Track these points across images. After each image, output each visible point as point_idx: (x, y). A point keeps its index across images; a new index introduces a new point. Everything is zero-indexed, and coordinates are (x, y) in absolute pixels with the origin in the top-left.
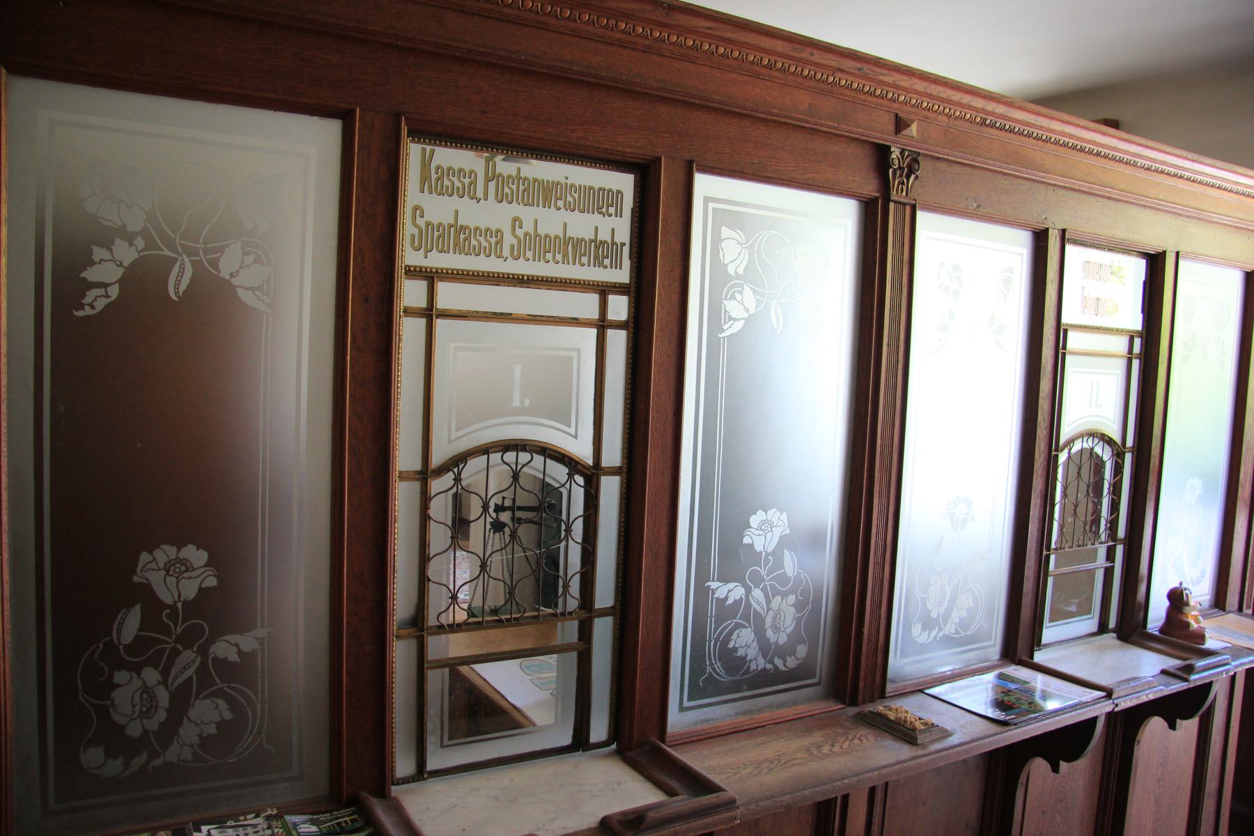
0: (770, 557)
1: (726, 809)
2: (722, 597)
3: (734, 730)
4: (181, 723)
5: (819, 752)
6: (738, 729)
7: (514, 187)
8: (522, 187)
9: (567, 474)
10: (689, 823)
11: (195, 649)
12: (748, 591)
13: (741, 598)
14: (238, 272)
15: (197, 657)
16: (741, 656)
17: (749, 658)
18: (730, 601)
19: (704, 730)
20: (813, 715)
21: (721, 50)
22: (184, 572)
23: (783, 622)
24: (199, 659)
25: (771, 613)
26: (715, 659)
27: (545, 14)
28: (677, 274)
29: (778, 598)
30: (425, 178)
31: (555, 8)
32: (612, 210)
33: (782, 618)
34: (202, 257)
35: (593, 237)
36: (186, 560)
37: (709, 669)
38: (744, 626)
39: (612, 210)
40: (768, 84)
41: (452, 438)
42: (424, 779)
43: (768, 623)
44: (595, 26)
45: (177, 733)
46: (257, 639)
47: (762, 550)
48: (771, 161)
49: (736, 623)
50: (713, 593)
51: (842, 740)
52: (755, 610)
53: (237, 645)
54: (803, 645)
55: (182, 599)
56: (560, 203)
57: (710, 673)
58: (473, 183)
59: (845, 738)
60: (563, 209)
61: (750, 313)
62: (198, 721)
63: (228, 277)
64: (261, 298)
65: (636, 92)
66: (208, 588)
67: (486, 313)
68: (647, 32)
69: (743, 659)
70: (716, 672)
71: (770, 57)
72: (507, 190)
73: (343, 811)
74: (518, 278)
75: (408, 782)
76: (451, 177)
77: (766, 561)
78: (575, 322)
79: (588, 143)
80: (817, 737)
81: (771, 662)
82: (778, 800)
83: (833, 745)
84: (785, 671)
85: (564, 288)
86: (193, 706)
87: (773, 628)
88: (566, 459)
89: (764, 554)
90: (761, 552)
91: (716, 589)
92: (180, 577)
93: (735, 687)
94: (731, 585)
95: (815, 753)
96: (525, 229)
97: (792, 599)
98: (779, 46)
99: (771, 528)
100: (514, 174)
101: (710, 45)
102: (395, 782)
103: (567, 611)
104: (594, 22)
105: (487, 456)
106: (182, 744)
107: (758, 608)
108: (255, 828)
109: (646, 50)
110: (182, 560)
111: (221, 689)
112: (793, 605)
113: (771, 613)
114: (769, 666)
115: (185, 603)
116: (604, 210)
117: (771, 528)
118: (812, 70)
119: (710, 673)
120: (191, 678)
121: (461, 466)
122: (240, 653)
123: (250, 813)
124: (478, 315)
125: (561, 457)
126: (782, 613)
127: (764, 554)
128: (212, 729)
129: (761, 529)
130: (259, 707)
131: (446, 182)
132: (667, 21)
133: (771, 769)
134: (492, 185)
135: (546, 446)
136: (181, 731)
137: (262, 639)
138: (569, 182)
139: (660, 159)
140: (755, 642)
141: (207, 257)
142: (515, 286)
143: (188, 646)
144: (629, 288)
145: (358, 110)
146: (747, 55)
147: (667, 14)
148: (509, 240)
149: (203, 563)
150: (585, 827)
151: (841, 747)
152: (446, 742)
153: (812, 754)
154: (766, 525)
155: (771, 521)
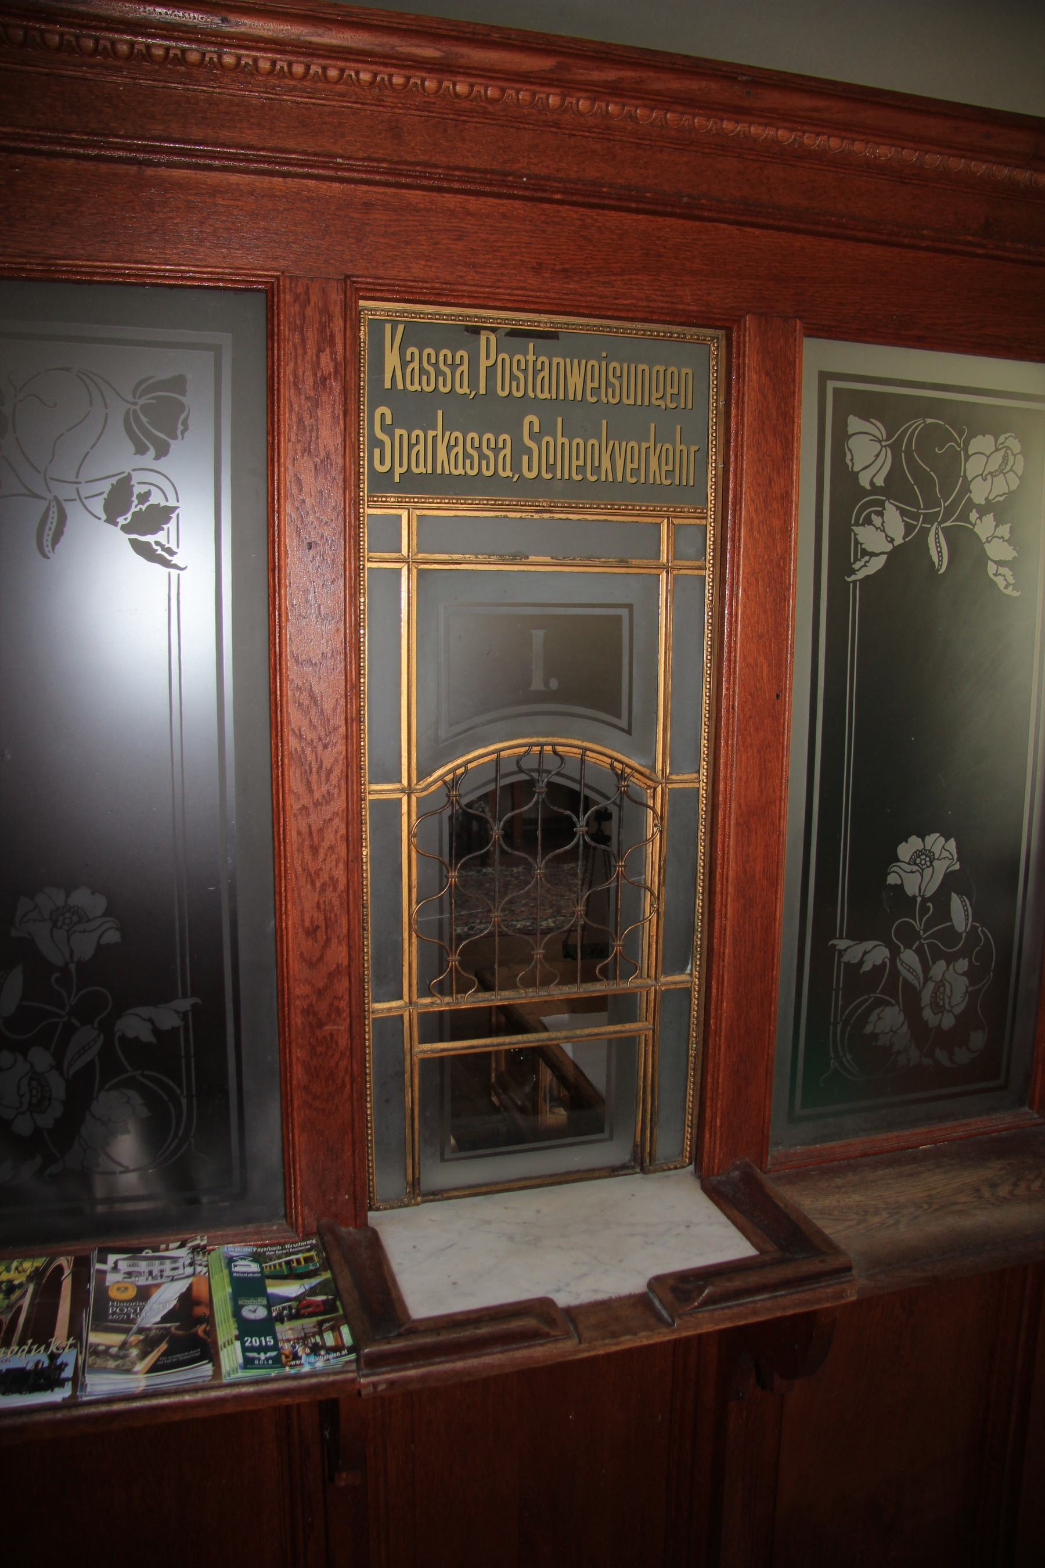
0: (930, 904)
2: (855, 961)
11: (96, 1025)
12: (895, 952)
13: (884, 964)
18: (867, 967)
22: (76, 924)
23: (950, 998)
24: (102, 1036)
25: (931, 986)
29: (942, 964)
38: (889, 1004)
43: (926, 996)
46: (177, 1012)
47: (917, 894)
52: (905, 980)
53: (150, 1020)
55: (75, 960)
61: (896, 543)
77: (924, 910)
83: (1015, 1185)
89: (919, 899)
90: (915, 897)
91: (846, 950)
94: (869, 945)
97: (963, 965)
99: (931, 862)
107: (910, 978)
108: (175, 1262)
112: (964, 974)
113: (931, 986)
122: (156, 1031)
126: (948, 986)
127: (919, 899)
129: (915, 864)
130: (184, 1101)
137: (185, 1014)
149: (100, 911)
154: (923, 857)
155: (930, 851)
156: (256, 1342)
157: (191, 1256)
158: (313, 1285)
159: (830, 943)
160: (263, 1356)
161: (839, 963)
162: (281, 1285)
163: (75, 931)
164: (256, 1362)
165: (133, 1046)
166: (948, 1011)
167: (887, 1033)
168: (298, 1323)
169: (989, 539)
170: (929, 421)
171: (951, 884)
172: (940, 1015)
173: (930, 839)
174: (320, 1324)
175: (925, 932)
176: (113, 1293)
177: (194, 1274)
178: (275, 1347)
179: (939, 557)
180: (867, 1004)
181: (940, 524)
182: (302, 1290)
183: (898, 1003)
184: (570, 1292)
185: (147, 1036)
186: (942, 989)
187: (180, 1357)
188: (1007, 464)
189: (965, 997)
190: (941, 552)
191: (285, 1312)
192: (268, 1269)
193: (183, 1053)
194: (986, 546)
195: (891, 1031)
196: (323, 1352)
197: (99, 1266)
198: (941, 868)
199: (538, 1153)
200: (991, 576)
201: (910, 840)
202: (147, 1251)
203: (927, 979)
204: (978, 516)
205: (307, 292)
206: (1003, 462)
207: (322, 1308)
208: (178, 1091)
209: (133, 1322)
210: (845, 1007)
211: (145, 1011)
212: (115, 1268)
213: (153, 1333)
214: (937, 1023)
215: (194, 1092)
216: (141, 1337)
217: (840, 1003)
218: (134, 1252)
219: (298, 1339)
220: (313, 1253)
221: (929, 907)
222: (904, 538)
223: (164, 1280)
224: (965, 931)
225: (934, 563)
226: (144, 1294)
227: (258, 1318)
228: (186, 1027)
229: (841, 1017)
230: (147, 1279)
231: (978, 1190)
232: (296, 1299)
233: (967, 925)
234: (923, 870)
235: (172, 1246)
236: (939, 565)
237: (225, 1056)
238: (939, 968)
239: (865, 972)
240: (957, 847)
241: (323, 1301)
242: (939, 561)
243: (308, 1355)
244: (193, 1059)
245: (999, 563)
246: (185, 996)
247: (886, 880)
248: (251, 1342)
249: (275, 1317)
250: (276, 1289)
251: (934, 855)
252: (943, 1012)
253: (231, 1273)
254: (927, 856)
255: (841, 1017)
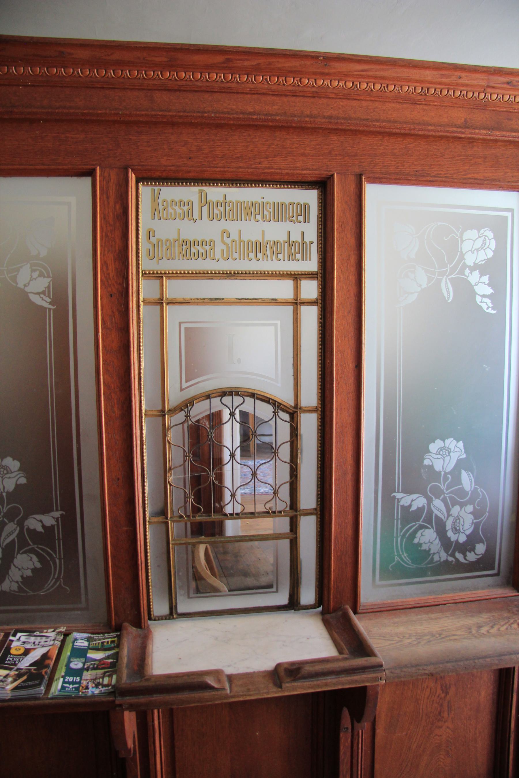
0: (449, 476)
1: (373, 671)
2: (407, 504)
3: (418, 605)
4: (9, 568)
5: (477, 632)
6: (421, 605)
7: (222, 209)
8: (227, 208)
9: (229, 414)
10: (339, 677)
11: (15, 522)
12: (430, 501)
13: (424, 506)
14: (29, 283)
15: (17, 527)
16: (425, 550)
17: (432, 552)
18: (414, 508)
19: (393, 603)
20: (490, 599)
21: (378, 86)
22: (6, 474)
23: (463, 525)
24: (18, 528)
25: (451, 519)
26: (402, 551)
27: (228, 82)
28: (353, 261)
29: (457, 508)
30: (155, 210)
31: (234, 76)
32: (301, 218)
33: (462, 523)
34: (6, 275)
35: (176, 237)
36: (7, 466)
37: (397, 558)
38: (427, 528)
39: (301, 218)
40: (425, 107)
41: (183, 387)
42: (173, 618)
43: (449, 525)
44: (269, 83)
45: (8, 573)
46: (54, 518)
47: (441, 470)
48: (433, 168)
49: (420, 524)
50: (399, 501)
51: (502, 623)
52: (436, 515)
53: (41, 521)
54: (481, 545)
55: (6, 490)
56: (259, 217)
57: (398, 561)
58: (191, 210)
59: (507, 621)
60: (261, 221)
61: (423, 287)
62: (20, 567)
63: (22, 287)
64: (44, 299)
65: (308, 128)
66: (21, 485)
67: (204, 299)
68: (312, 81)
69: (427, 552)
70: (403, 561)
71: (422, 85)
72: (216, 211)
73: (112, 634)
74: (227, 273)
75: (162, 619)
76: (173, 206)
77: (446, 479)
78: (274, 302)
79: (273, 170)
80: (484, 617)
81: (453, 555)
82: (421, 668)
83: (492, 627)
84: (465, 564)
85: (264, 278)
86: (16, 557)
87: (454, 530)
88: (271, 401)
89: (443, 473)
90: (440, 472)
91: (401, 499)
92: (4, 477)
93: (421, 573)
94: (414, 496)
95: (474, 631)
96: (232, 237)
97: (470, 508)
98: (429, 75)
99: (449, 453)
100: (221, 199)
101: (367, 84)
102: (153, 618)
103: (235, 512)
104: (267, 81)
105: (209, 400)
106: (11, 580)
107: (439, 515)
108: (47, 638)
109: (315, 95)
110: (4, 466)
111: (33, 548)
112: (471, 513)
113: (451, 519)
114: (450, 559)
115: (8, 493)
116: (294, 219)
117: (449, 453)
118: (464, 90)
119: (398, 561)
120: (13, 540)
121: (189, 408)
122: (44, 526)
123: (50, 628)
124: (198, 301)
125: (268, 400)
126: (461, 519)
127: (443, 473)
128: (29, 573)
129: (440, 454)
130: (57, 561)
131: (171, 211)
132: (326, 71)
133: (429, 642)
134: (205, 209)
135: (255, 392)
136: (10, 572)
137: (57, 519)
138: (265, 201)
139: (333, 175)
140: (438, 540)
141: (9, 275)
142: (225, 279)
143: (11, 520)
144: (317, 274)
145: (98, 168)
146: (401, 87)
147: (325, 65)
148: (220, 247)
149: (16, 468)
150: (262, 669)
151: (499, 630)
152: (192, 595)
153: (470, 632)
154: (444, 451)
155: (448, 448)
156: (71, 679)
157: (55, 636)
158: (110, 654)
159: (392, 495)
160: (71, 686)
161: (398, 505)
162: (95, 653)
163: (5, 478)
164: (67, 689)
165: (33, 533)
166: (462, 533)
167: (427, 543)
168: (94, 672)
169: (477, 284)
170: (440, 223)
171: (460, 465)
172: (458, 534)
173: (448, 441)
174: (105, 673)
175: (447, 490)
176: (13, 651)
177: (53, 645)
178: (79, 683)
179: (448, 293)
180: (414, 528)
181: (447, 276)
182: (104, 656)
183: (433, 528)
184: (235, 667)
185: (40, 529)
186: (458, 521)
187: (33, 683)
188: (485, 244)
189: (472, 524)
190: (449, 291)
191: (91, 666)
192: (92, 645)
193: (57, 538)
194: (475, 287)
195: (429, 542)
196: (100, 687)
197: (11, 638)
198: (454, 457)
199: (243, 596)
200: (478, 303)
201: (436, 442)
202: (37, 632)
203: (449, 515)
204: (469, 272)
205: (109, 175)
206: (483, 243)
207: (109, 666)
208: (54, 556)
209: (15, 665)
210: (402, 529)
211: (39, 517)
212: (19, 640)
213: (24, 670)
214: (456, 539)
215: (62, 557)
216: (17, 673)
217: (399, 526)
218: (30, 632)
219: (91, 679)
220: (116, 639)
221: (449, 477)
222: (427, 284)
223: (39, 646)
224: (470, 490)
225: (445, 297)
226: (27, 652)
227: (77, 668)
228: (58, 525)
229: (400, 533)
230: (31, 646)
231: (470, 629)
232: (100, 660)
233: (471, 487)
234: (444, 457)
235: (50, 630)
236: (448, 298)
237: (76, 538)
238: (456, 510)
239: (413, 511)
240: (464, 446)
241: (111, 662)
242: (448, 296)
243: (93, 687)
244: (61, 541)
245: (484, 296)
246: (57, 510)
247: (423, 463)
248: (69, 679)
249: (86, 668)
250: (92, 655)
251: (450, 450)
252: (459, 533)
253: (73, 645)
254: (446, 450)
255: (400, 533)
